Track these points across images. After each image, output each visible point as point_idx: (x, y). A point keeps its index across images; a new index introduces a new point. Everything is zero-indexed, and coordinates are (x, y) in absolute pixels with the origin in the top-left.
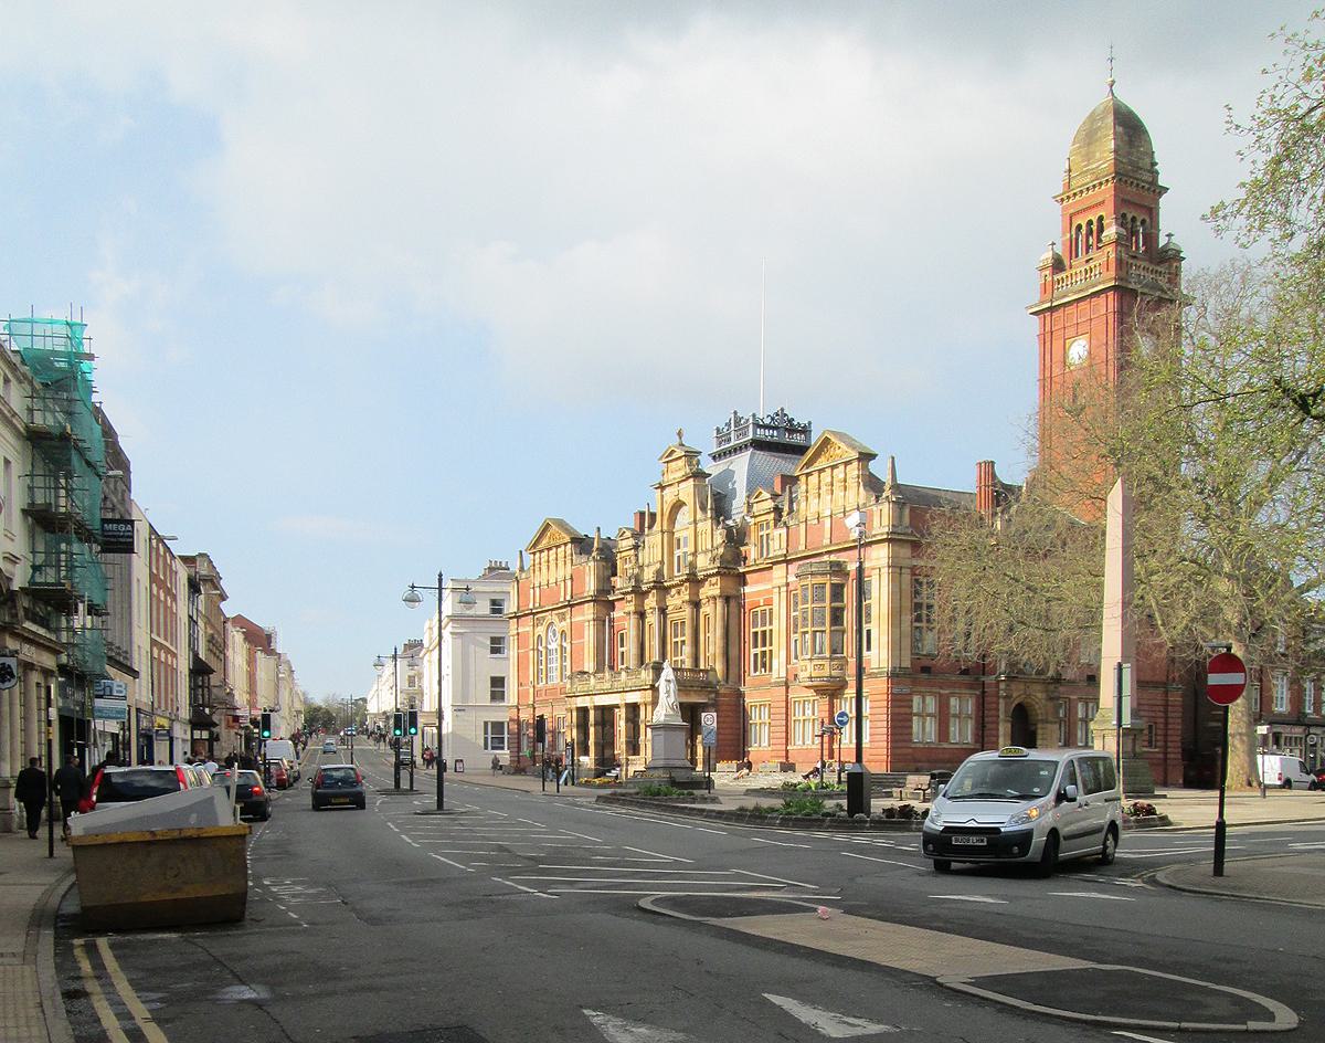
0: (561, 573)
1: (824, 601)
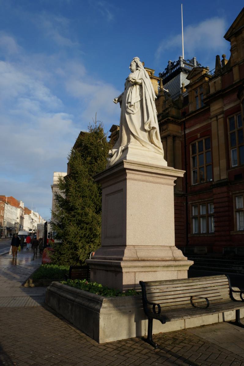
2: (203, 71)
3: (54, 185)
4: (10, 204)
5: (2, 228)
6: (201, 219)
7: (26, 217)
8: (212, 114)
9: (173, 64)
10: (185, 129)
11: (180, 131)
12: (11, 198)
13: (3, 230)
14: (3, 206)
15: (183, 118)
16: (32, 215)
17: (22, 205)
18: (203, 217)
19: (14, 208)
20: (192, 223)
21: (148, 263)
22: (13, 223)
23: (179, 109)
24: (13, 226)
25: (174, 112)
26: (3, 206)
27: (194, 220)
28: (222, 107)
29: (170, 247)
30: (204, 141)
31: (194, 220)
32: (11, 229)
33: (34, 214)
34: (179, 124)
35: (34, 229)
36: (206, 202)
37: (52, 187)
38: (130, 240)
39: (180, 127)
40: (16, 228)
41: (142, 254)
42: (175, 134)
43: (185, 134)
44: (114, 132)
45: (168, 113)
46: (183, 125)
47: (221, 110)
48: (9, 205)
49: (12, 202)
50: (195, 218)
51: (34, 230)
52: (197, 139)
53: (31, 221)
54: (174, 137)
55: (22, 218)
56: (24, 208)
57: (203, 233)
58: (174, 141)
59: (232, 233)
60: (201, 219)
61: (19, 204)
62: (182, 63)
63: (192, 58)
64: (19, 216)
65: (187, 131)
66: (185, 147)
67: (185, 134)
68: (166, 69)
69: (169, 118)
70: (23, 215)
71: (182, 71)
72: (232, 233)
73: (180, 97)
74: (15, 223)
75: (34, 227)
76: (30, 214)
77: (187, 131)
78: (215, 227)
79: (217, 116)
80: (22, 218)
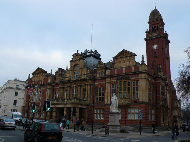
0: (41, 79)
1: (126, 85)
58: (91, 86)
59: (126, 120)
79: (108, 83)
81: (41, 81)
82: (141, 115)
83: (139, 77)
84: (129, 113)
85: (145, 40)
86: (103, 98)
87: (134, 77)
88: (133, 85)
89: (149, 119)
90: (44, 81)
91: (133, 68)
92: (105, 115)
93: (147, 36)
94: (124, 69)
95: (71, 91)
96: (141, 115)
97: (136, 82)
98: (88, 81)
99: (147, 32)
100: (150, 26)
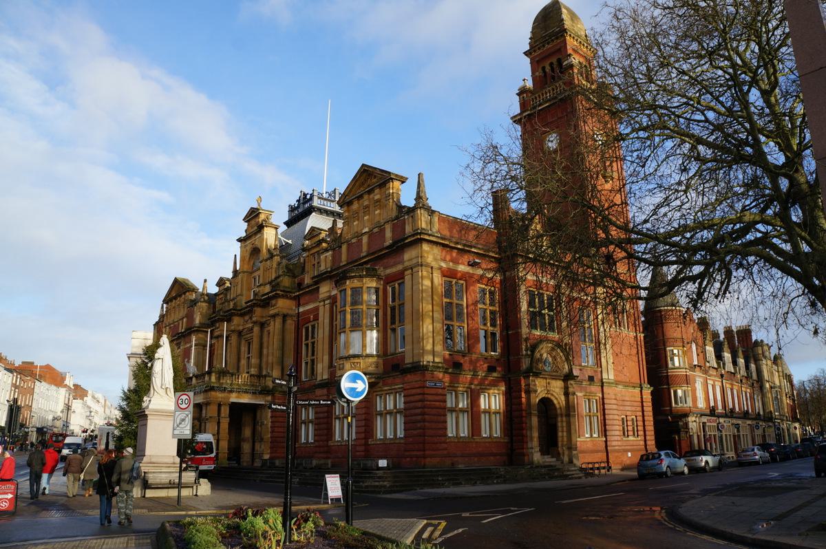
2: (320, 233)
3: (132, 354)
4: (45, 381)
5: (26, 430)
6: (388, 417)
7: (77, 405)
8: (321, 296)
9: (306, 196)
10: (299, 305)
11: (294, 308)
12: (48, 367)
13: (30, 433)
14: (31, 385)
15: (297, 292)
16: (88, 399)
17: (69, 382)
18: (390, 413)
19: (53, 387)
20: (301, 429)
21: (156, 465)
22: (50, 418)
23: (294, 276)
24: (50, 424)
25: (286, 282)
26: (31, 385)
27: (379, 418)
28: (329, 291)
29: (173, 456)
30: (310, 327)
31: (379, 418)
32: (45, 430)
33: (93, 397)
34: (294, 298)
35: (92, 428)
36: (393, 391)
37: (129, 358)
38: (147, 453)
39: (294, 302)
40: (55, 427)
41: (153, 460)
42: (285, 311)
43: (299, 313)
44: (222, 288)
45: (278, 284)
46: (298, 300)
47: (328, 294)
48: (43, 383)
49: (48, 376)
50: (304, 422)
51: (92, 431)
52: (310, 322)
53: (88, 413)
54: (285, 317)
55: (68, 408)
56: (73, 388)
57: (389, 439)
58: (284, 321)
59: (330, 443)
60: (388, 417)
61: (63, 379)
62: (315, 199)
63: (333, 190)
64: (61, 406)
65: (301, 310)
66: (298, 328)
67: (299, 313)
68: (297, 201)
69: (278, 292)
70: (70, 402)
71: (315, 211)
72: (330, 443)
73: (299, 259)
74: (55, 419)
75: (93, 424)
76: (85, 398)
77: (301, 310)
78: (356, 433)
79: (324, 301)
80: (68, 408)
81: (181, 322)
82: (183, 420)
83: (402, 262)
84: (452, 410)
85: (517, 120)
86: (313, 361)
87: (391, 266)
88: (390, 299)
89: (445, 435)
90: (187, 321)
91: (388, 234)
92: (276, 429)
93: (523, 105)
94: (365, 239)
95: (244, 349)
96: (183, 420)
97: (396, 284)
98: (274, 302)
99: (522, 92)
100: (535, 64)
